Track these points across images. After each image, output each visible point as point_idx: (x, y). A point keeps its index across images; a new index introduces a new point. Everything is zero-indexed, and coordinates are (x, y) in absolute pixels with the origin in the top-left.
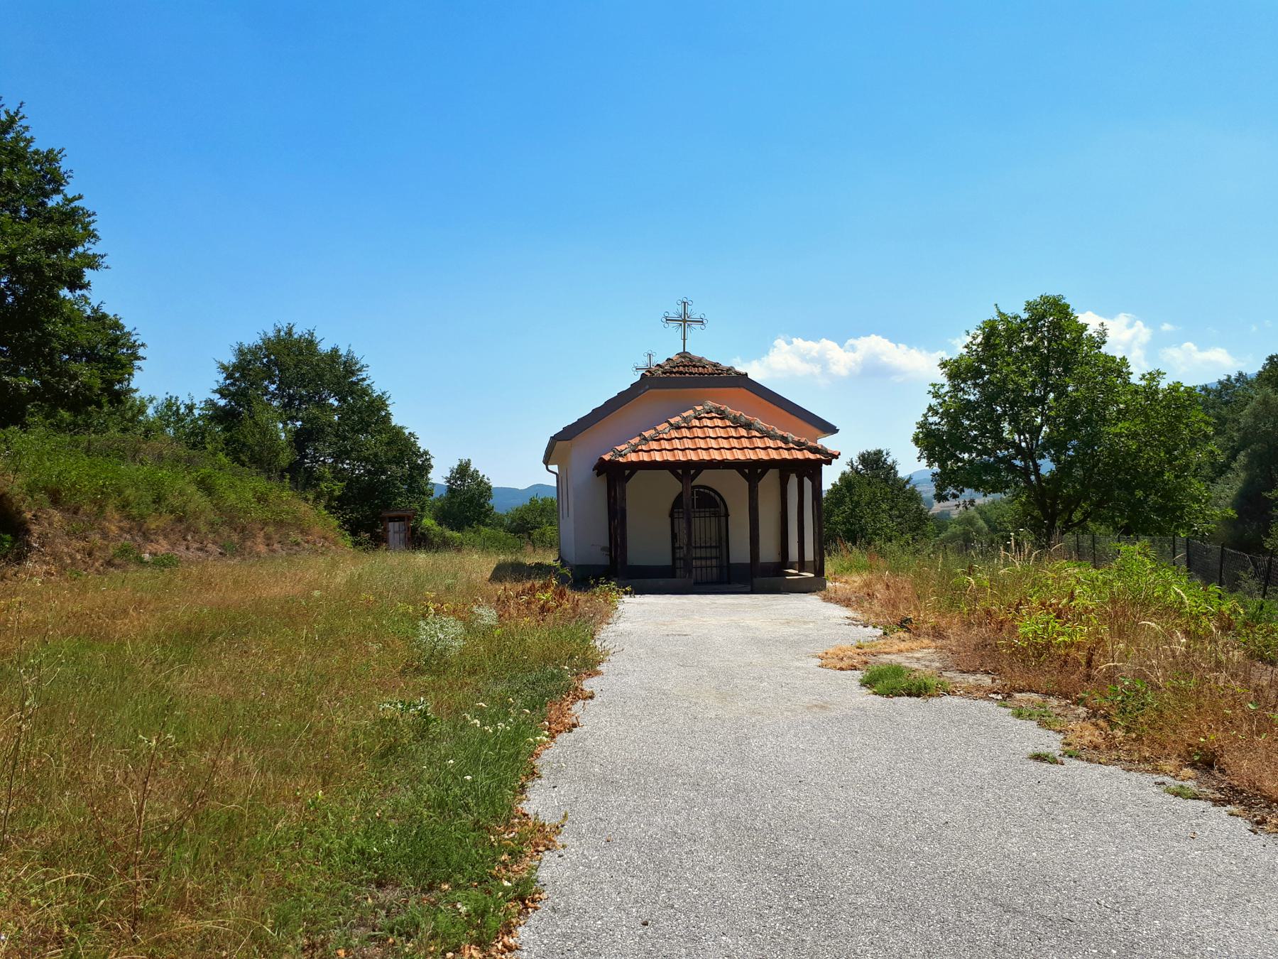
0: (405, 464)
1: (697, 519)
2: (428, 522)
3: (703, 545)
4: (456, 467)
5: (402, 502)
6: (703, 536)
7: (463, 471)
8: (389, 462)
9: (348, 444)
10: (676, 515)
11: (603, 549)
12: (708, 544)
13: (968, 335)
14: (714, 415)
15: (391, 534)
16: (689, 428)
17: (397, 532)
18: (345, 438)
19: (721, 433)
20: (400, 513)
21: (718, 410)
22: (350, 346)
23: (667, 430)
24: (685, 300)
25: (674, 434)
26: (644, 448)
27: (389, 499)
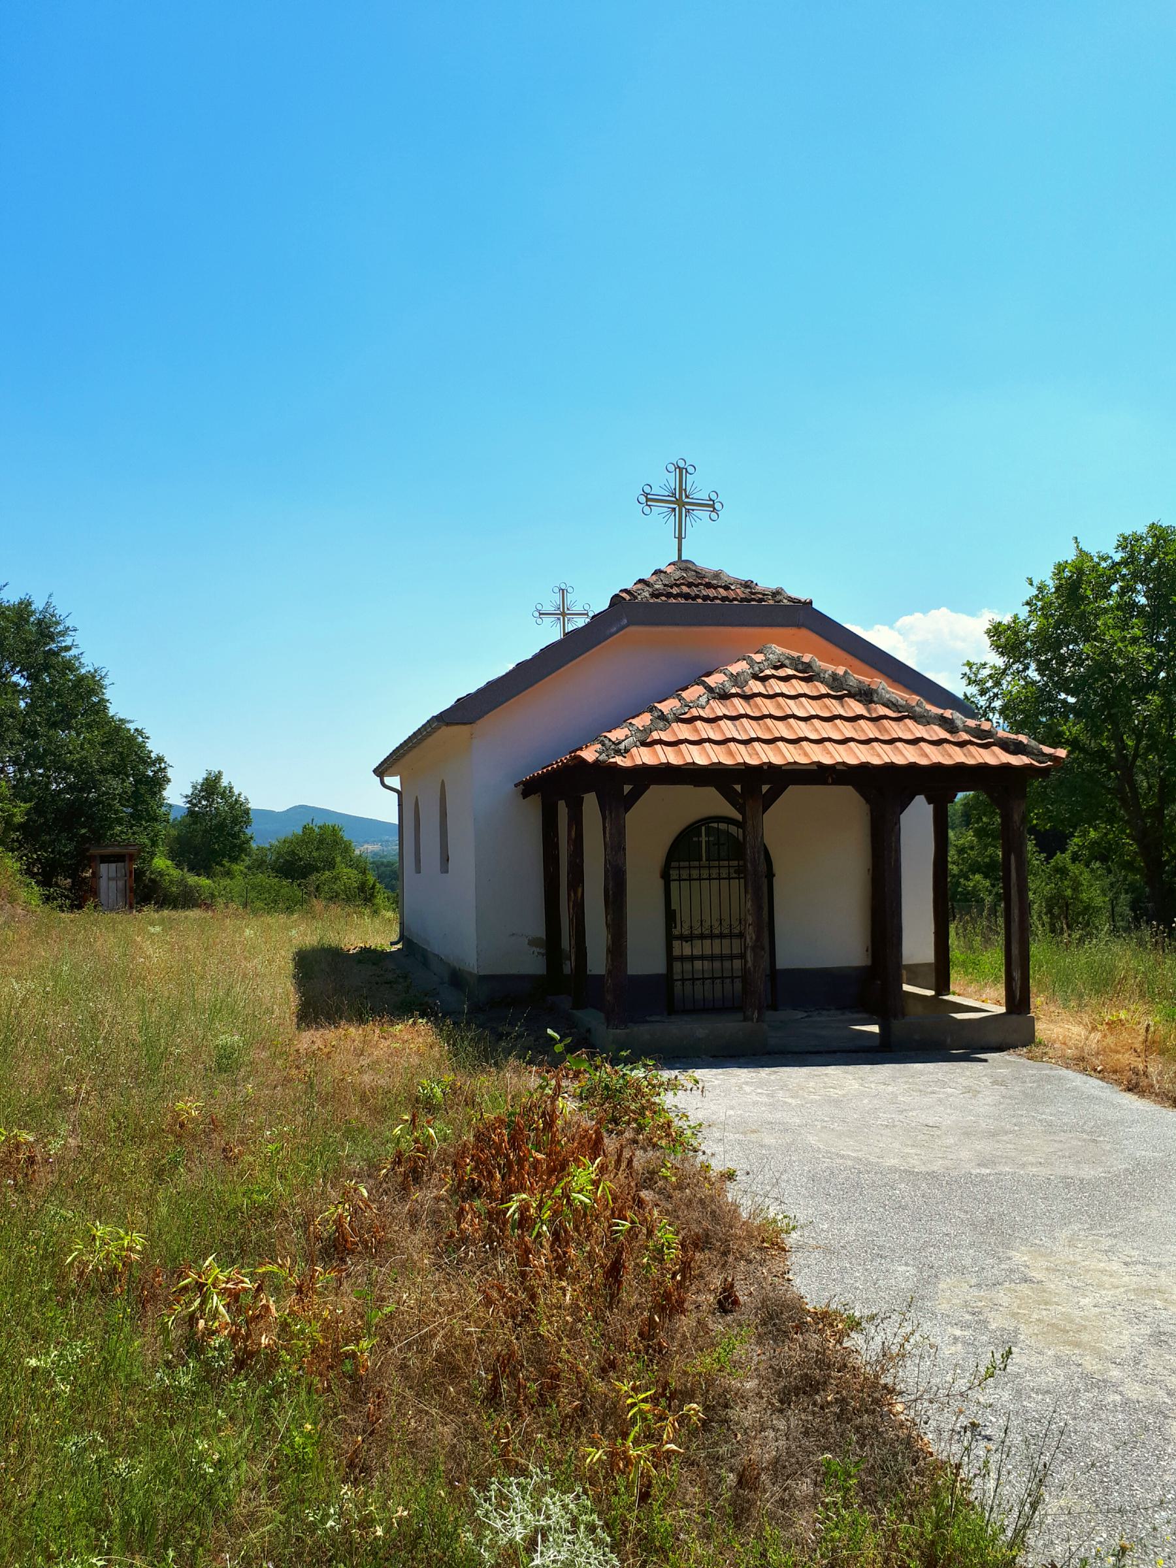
0: (128, 777)
1: (685, 884)
2: (161, 862)
3: (726, 931)
4: (200, 781)
5: (122, 832)
6: (706, 917)
7: (211, 787)
8: (103, 771)
9: (41, 743)
10: (674, 874)
11: (533, 942)
12: (717, 932)
13: (1031, 584)
14: (790, 672)
15: (103, 882)
16: (747, 698)
17: (113, 879)
18: (35, 736)
19: (812, 708)
20: (117, 850)
21: (796, 663)
22: (50, 596)
23: (703, 700)
24: (681, 464)
25: (719, 709)
26: (665, 736)
27: (102, 827)
